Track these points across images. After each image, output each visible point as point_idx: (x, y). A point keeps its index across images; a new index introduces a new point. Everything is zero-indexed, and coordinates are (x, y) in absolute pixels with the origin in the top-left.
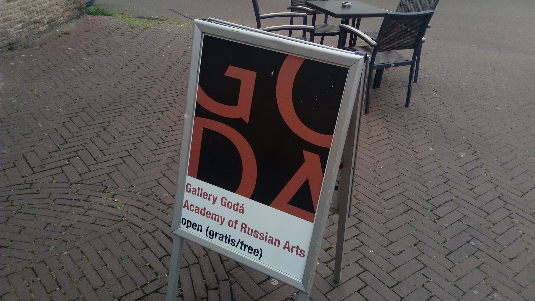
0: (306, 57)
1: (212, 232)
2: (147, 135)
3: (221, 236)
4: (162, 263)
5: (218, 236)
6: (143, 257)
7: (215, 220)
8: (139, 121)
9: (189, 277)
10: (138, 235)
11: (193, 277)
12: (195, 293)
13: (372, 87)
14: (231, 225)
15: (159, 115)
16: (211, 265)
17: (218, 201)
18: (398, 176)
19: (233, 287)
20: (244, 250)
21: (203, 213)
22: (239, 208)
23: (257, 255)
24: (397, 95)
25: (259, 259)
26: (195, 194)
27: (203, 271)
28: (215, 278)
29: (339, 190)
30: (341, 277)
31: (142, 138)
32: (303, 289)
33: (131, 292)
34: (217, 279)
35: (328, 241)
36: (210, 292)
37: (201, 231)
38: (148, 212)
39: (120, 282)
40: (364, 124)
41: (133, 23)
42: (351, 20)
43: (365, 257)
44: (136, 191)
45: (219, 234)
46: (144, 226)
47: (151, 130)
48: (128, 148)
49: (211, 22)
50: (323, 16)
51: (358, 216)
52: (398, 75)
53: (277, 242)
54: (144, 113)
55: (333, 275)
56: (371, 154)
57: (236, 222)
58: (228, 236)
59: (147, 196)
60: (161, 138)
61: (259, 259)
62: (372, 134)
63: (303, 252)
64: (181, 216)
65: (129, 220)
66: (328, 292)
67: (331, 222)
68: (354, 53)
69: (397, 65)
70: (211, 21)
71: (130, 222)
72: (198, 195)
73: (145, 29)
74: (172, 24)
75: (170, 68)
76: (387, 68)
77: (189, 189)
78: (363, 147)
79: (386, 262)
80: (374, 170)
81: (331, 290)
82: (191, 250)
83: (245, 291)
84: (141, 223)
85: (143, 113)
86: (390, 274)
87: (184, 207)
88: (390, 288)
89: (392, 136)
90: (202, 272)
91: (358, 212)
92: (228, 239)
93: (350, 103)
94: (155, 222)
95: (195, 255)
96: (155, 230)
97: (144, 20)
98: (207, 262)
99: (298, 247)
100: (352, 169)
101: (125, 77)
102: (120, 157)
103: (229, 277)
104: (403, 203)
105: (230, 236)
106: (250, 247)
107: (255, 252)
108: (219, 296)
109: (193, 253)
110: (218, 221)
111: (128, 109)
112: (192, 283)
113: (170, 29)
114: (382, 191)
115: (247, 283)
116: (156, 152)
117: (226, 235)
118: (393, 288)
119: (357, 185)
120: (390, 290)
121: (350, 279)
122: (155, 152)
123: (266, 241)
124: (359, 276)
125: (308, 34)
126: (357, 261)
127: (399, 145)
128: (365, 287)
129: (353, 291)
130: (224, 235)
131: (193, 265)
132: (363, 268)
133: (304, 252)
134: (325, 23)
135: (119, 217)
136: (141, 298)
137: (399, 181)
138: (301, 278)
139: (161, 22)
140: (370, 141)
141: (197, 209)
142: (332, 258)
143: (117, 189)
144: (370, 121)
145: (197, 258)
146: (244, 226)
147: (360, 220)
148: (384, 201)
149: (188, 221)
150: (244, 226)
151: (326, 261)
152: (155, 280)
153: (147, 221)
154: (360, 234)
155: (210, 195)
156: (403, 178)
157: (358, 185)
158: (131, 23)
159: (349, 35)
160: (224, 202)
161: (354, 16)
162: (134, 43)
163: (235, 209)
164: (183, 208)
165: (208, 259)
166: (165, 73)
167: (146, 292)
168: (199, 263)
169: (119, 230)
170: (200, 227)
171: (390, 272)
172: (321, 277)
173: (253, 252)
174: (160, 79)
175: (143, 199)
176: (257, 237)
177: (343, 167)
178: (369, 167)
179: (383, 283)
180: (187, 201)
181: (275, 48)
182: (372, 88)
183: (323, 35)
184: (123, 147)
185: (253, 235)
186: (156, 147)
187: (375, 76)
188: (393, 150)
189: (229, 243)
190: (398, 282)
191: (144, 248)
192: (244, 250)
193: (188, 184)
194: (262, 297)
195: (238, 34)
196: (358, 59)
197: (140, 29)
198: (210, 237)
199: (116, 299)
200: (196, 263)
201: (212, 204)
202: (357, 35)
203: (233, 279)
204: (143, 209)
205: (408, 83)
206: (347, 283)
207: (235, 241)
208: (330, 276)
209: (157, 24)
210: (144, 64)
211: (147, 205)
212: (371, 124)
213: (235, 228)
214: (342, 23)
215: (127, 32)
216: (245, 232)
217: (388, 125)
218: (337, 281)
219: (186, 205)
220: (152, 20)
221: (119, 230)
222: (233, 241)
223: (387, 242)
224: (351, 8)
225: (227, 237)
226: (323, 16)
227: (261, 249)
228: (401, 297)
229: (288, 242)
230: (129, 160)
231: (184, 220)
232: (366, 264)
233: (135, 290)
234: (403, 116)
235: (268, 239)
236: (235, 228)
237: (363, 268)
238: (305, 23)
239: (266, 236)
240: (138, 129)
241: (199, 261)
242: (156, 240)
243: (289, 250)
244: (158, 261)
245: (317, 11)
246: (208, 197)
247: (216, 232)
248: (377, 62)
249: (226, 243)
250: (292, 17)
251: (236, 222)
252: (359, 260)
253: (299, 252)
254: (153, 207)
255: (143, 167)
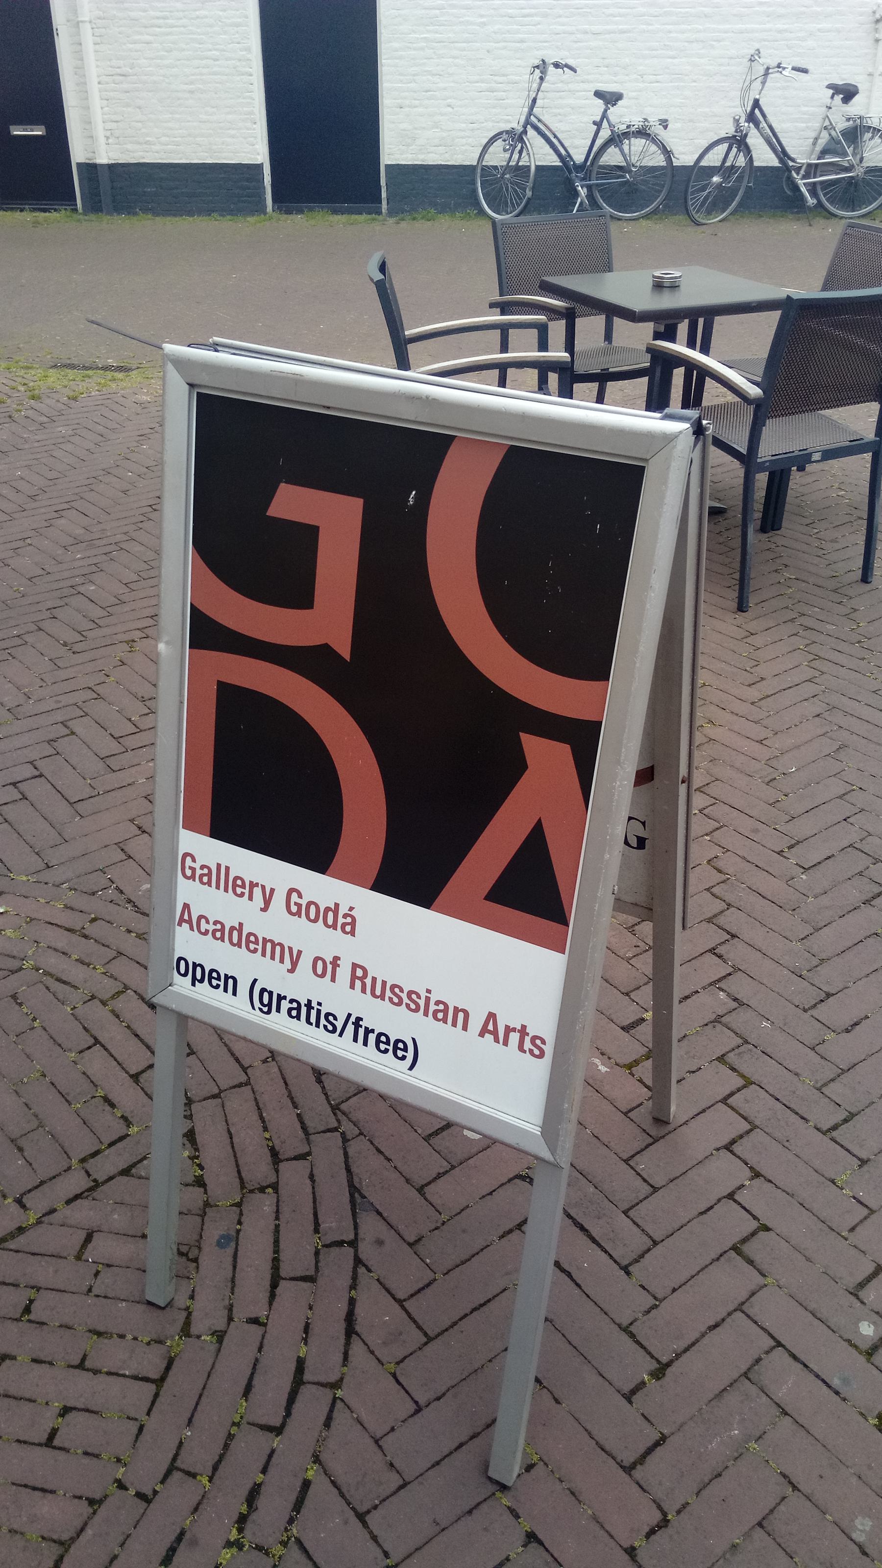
0: (512, 438)
1: (266, 996)
2: (87, 715)
3: (295, 1005)
4: (142, 1089)
5: (285, 1005)
6: (84, 1073)
7: (273, 958)
8: (63, 674)
9: (222, 1126)
10: (69, 1009)
11: (233, 1124)
12: (239, 1172)
13: (759, 527)
14: (320, 971)
15: (121, 651)
16: (286, 1088)
17: (279, 901)
18: (844, 795)
19: (351, 1152)
20: (365, 1043)
21: (235, 940)
22: (341, 920)
23: (403, 1058)
24: (837, 546)
25: (411, 1068)
26: (209, 883)
27: (261, 1106)
28: (298, 1126)
29: (647, 847)
30: (673, 1108)
31: (74, 721)
32: (546, 1154)
33: (54, 1177)
34: (304, 1128)
35: (634, 1001)
36: (282, 1166)
37: (234, 994)
38: (96, 941)
39: (20, 1149)
40: (736, 642)
41: (39, 383)
42: (683, 328)
43: (746, 1042)
44: (58, 880)
45: (288, 999)
46: (85, 982)
47: (99, 697)
48: (34, 755)
49: (216, 351)
50: (599, 320)
51: (721, 920)
52: (837, 485)
53: (461, 1015)
54: (76, 648)
55: (650, 1102)
56: (758, 732)
57: (336, 961)
58: (314, 1004)
59: (93, 894)
60: (130, 720)
61: (411, 1068)
62: (761, 670)
63: (538, 1042)
64: (174, 950)
65: (41, 967)
66: (638, 1153)
67: (640, 943)
68: (658, 415)
69: (829, 454)
70: (215, 347)
71: (44, 971)
72: (218, 887)
73: (75, 399)
74: (152, 378)
75: (150, 509)
76: (801, 469)
77: (190, 868)
78: (732, 713)
79: (812, 1054)
80: (767, 780)
81: (647, 1147)
82: (226, 1045)
83: (389, 1160)
84: (77, 973)
85: (74, 649)
86: (824, 1090)
87: (180, 924)
88: (824, 1133)
89: (823, 673)
90: (259, 1109)
91: (721, 909)
92: (313, 1013)
93: (653, 576)
94: (117, 968)
95: (237, 1060)
96: (119, 993)
97: (71, 373)
98: (272, 1079)
99: (524, 1027)
100: (683, 782)
101: (21, 544)
102: (12, 781)
103: (338, 1121)
104: (860, 874)
105: (319, 1004)
106: (380, 1034)
107: (398, 1048)
108: (312, 1177)
109: (233, 1054)
110: (282, 961)
111: (29, 638)
112: (232, 1143)
113: (147, 394)
114: (793, 842)
115: (392, 1136)
116: (114, 763)
117: (309, 1001)
118: (834, 1134)
119: (717, 829)
120: (826, 1139)
121: (704, 1111)
122: (111, 762)
123: (426, 1014)
124: (729, 1101)
125: (553, 378)
126: (723, 1055)
127: (845, 700)
128: (748, 1132)
129: (713, 1148)
130: (303, 1002)
131: (233, 1090)
132: (743, 1076)
133: (543, 1042)
134: (606, 343)
135: (14, 957)
136: (82, 1193)
137: (848, 810)
138: (540, 1123)
139: (120, 375)
140: (754, 693)
141: (219, 926)
142: (430, 1142)
143: (5, 876)
144: (753, 632)
145: (245, 1069)
146: (359, 973)
147: (728, 933)
148: (803, 870)
149: (195, 965)
150: (359, 973)
151: (629, 1059)
152: (121, 1139)
153: (94, 968)
154: (730, 974)
155: (253, 885)
156: (859, 799)
157: (722, 827)
158: (31, 384)
159: (679, 374)
160: (296, 904)
161: (693, 314)
162: (43, 443)
163: (330, 921)
164: (177, 928)
165: (276, 1070)
166: (134, 527)
167: (94, 1176)
168: (250, 1084)
169: (14, 997)
170: (231, 981)
171: (825, 1085)
172: (614, 1109)
173: (391, 1048)
174: (124, 546)
175: (82, 902)
176: (400, 1004)
177: (653, 779)
178: (755, 772)
179: (802, 1118)
180: (186, 906)
181: (413, 418)
182: (756, 531)
183: (603, 378)
184: (19, 752)
185: (387, 998)
186: (114, 747)
187: (763, 493)
188: (826, 715)
189: (318, 1026)
190: (850, 1112)
191: (87, 1046)
192: (365, 1043)
193: (186, 855)
194: (439, 1176)
195: (298, 381)
196: (671, 435)
197: (58, 401)
198: (261, 1010)
199: (10, 1200)
200: (240, 1085)
201: (262, 910)
202: (705, 373)
203: (353, 1126)
204: (83, 931)
205: (866, 508)
206: (693, 1123)
207: (335, 1018)
208: (641, 1104)
209: (109, 383)
210: (73, 504)
211: (93, 920)
212: (758, 640)
213: (333, 979)
214: (657, 336)
215: (20, 411)
216: (364, 991)
217: (809, 642)
218: (664, 1119)
219: (186, 917)
220: (94, 371)
221: (14, 997)
222: (331, 1018)
223: (811, 996)
224: (682, 288)
225: (313, 1008)
226: (599, 320)
227: (414, 1040)
228: (859, 1159)
229: (492, 1016)
230: (37, 790)
231: (182, 963)
232: (750, 1064)
233: (65, 1171)
234: (855, 610)
235: (432, 1007)
236: (333, 979)
237: (743, 1076)
238: (543, 345)
239: (428, 999)
240: (59, 698)
241: (249, 1078)
242: (122, 1022)
243: (497, 1040)
244: (129, 1081)
245: (579, 308)
246: (247, 891)
247: (279, 995)
248: (767, 450)
249: (311, 1024)
250: (504, 329)
251: (336, 961)
252: (728, 1052)
253: (528, 1045)
254: (112, 924)
255: (79, 807)
